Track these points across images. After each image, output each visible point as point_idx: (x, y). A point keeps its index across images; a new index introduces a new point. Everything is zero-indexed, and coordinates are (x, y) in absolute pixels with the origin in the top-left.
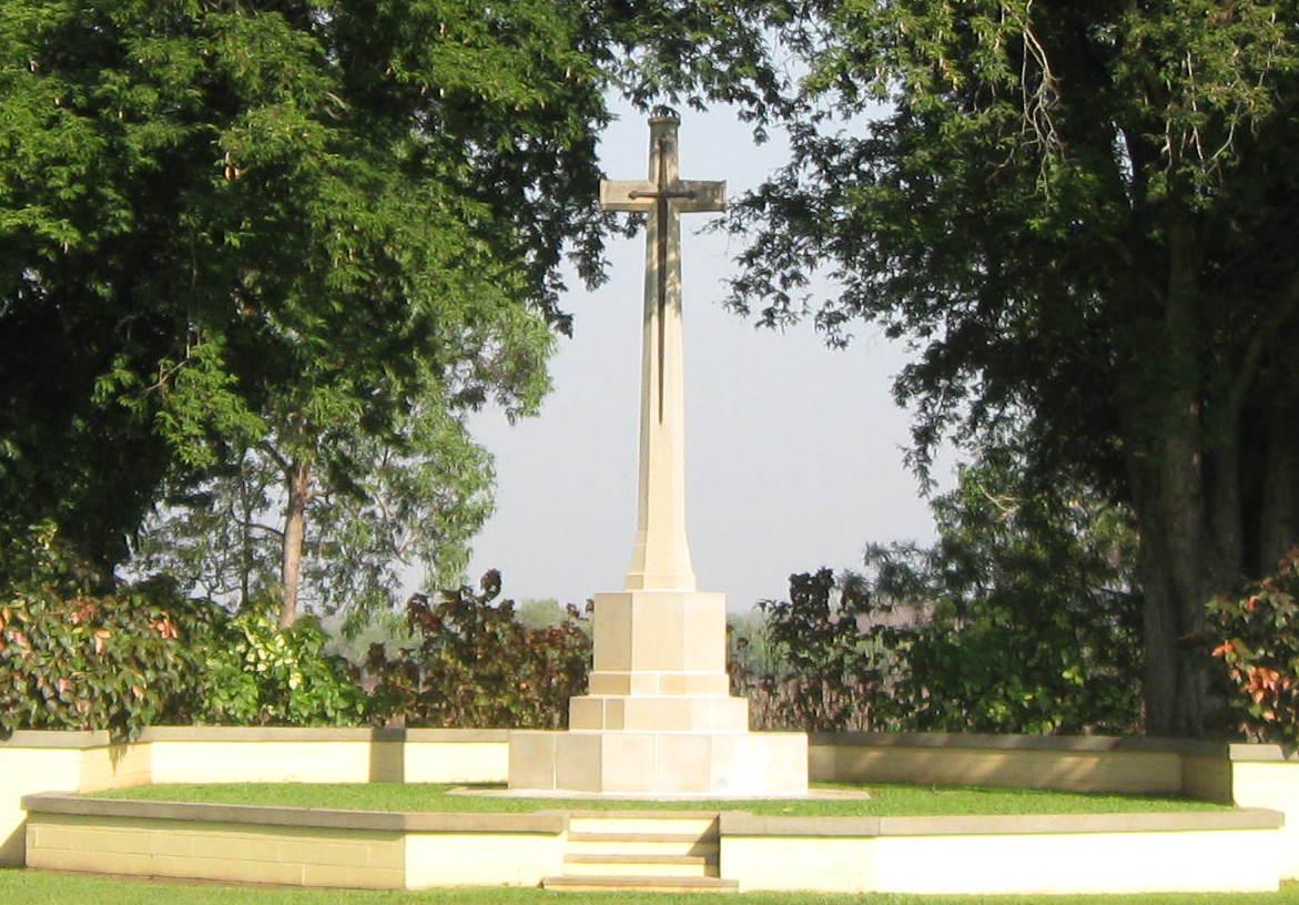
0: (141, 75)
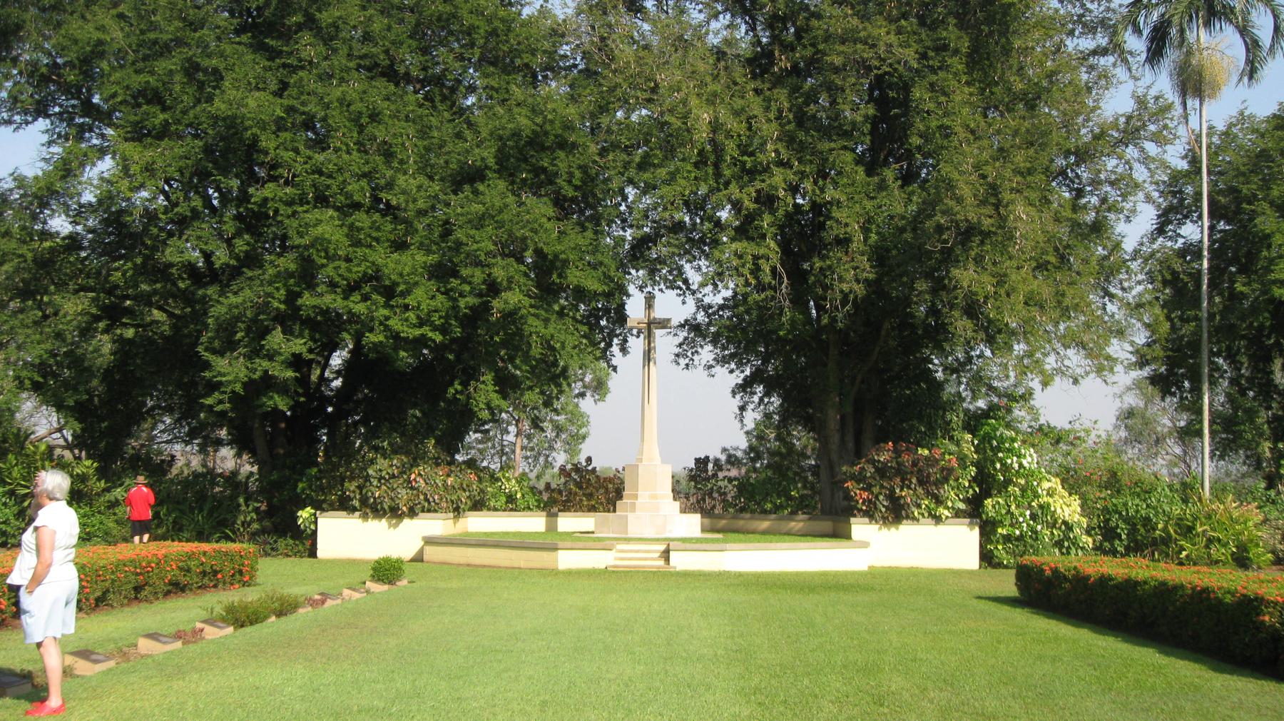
0: (465, 281)
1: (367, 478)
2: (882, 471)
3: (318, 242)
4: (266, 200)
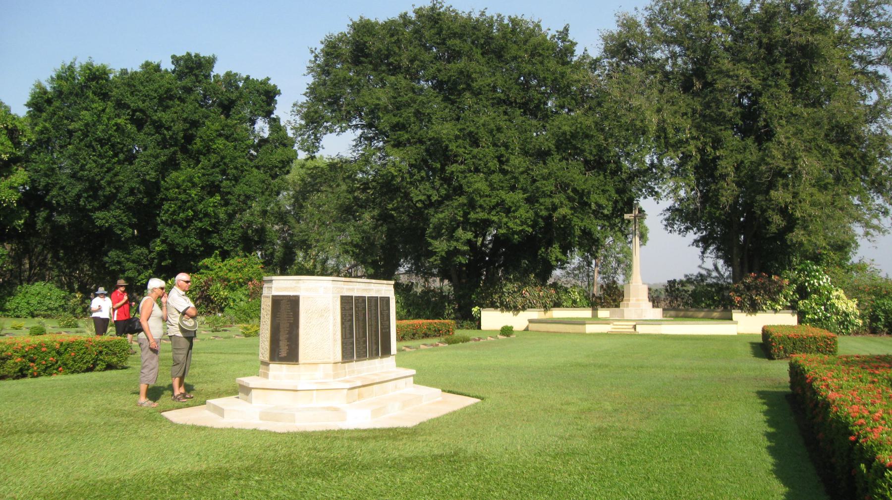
0: (541, 204)
1: (503, 293)
2: (748, 288)
3: (477, 191)
4: (453, 172)
